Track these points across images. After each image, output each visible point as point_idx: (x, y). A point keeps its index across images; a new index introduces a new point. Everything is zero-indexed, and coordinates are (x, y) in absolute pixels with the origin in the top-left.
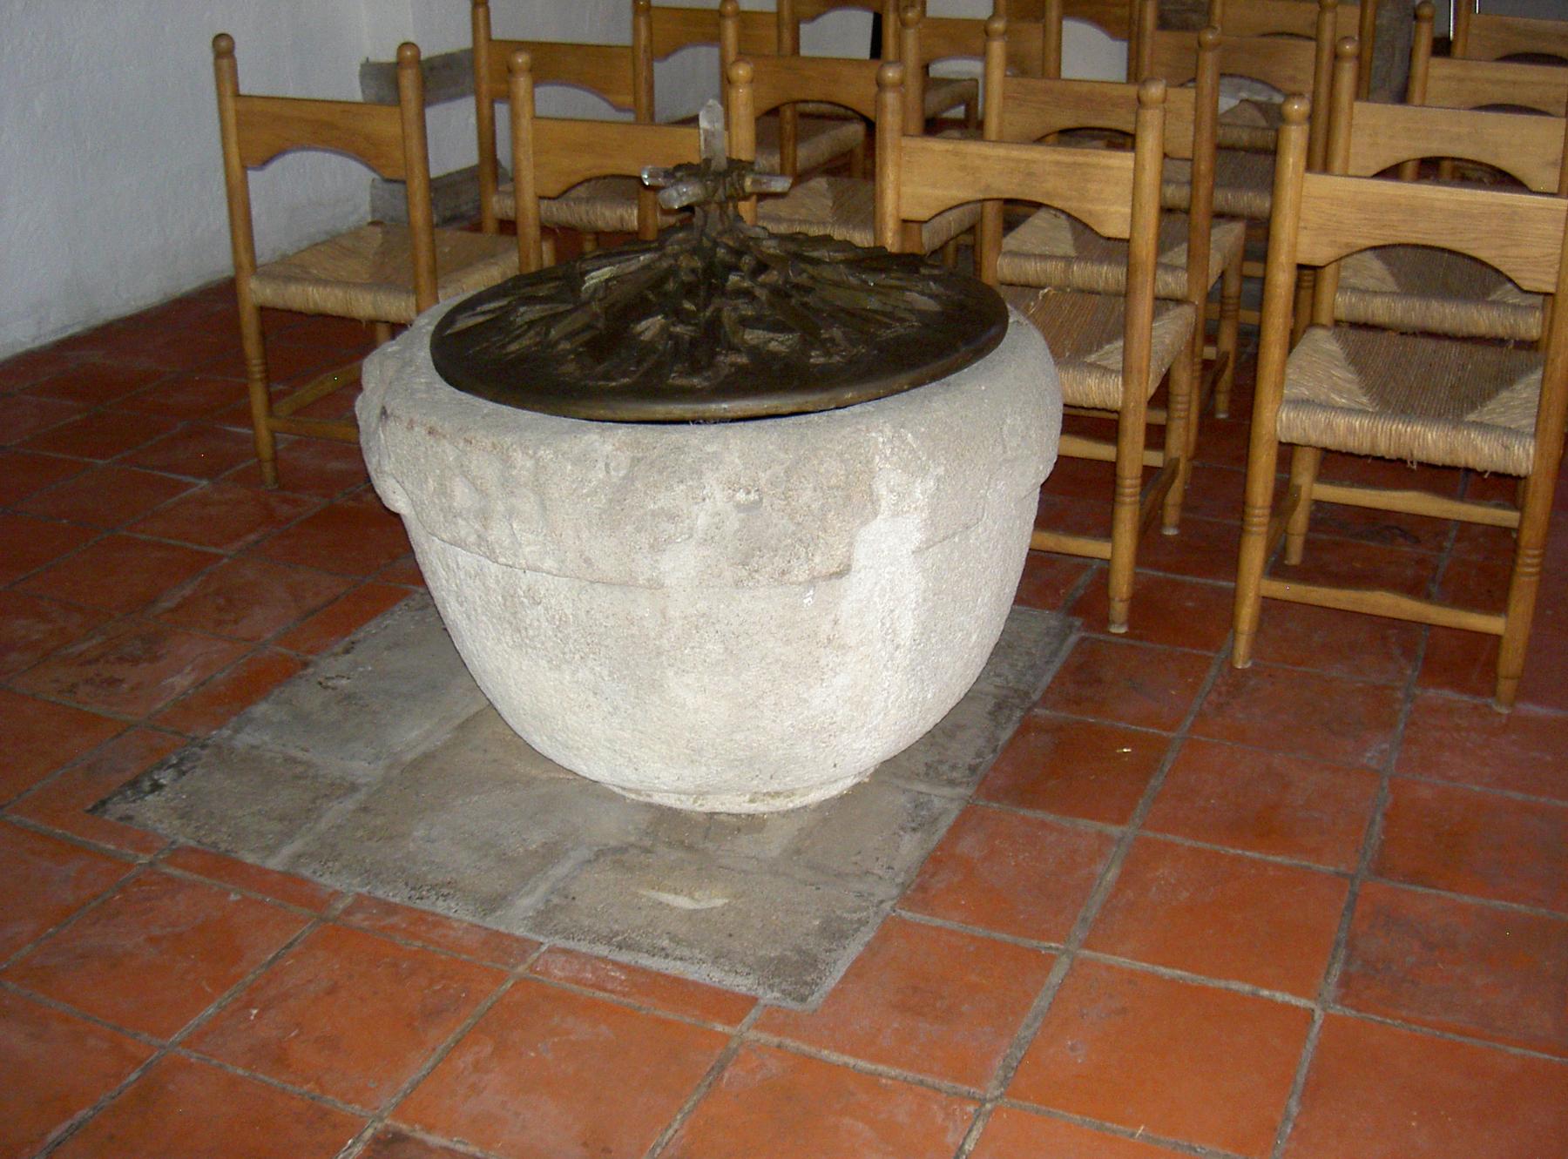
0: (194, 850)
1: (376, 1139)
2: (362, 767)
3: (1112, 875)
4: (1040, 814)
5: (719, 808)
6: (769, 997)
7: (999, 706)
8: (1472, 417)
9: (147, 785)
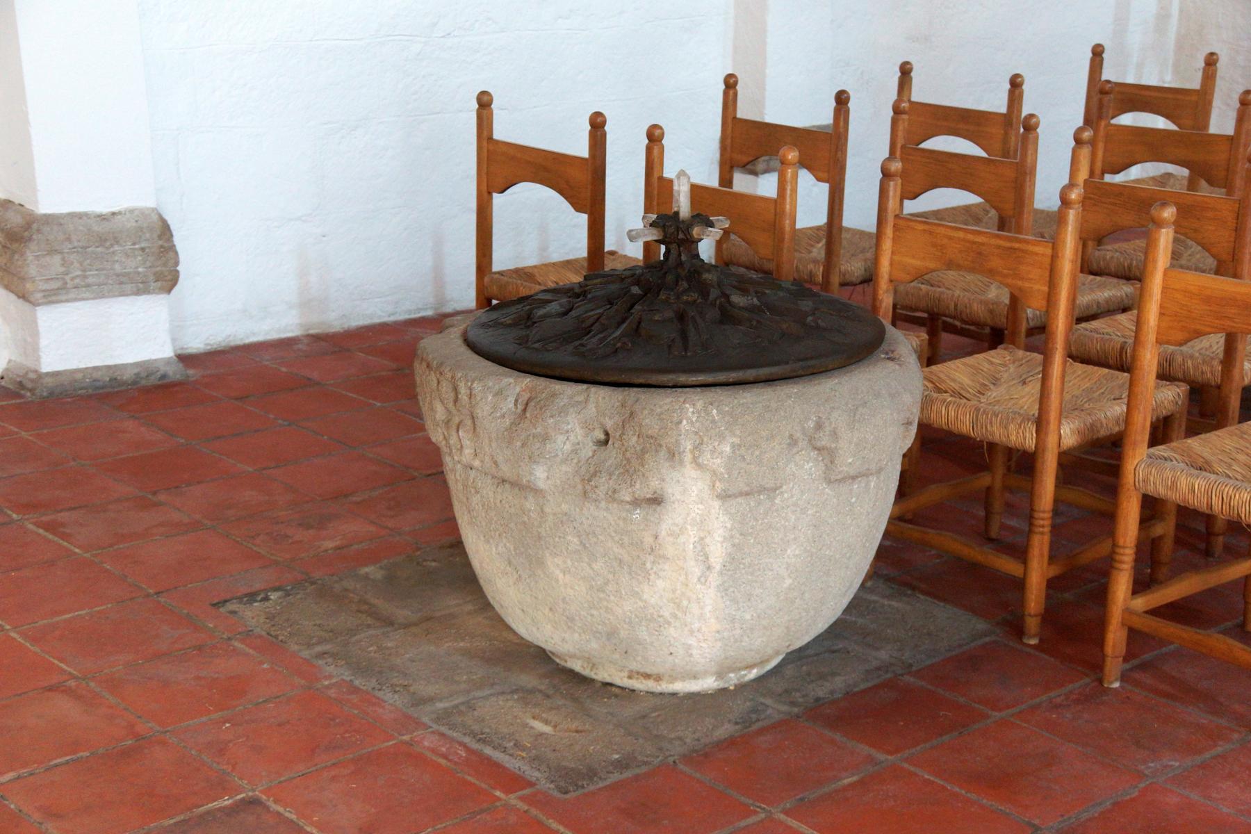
6: (545, 785)
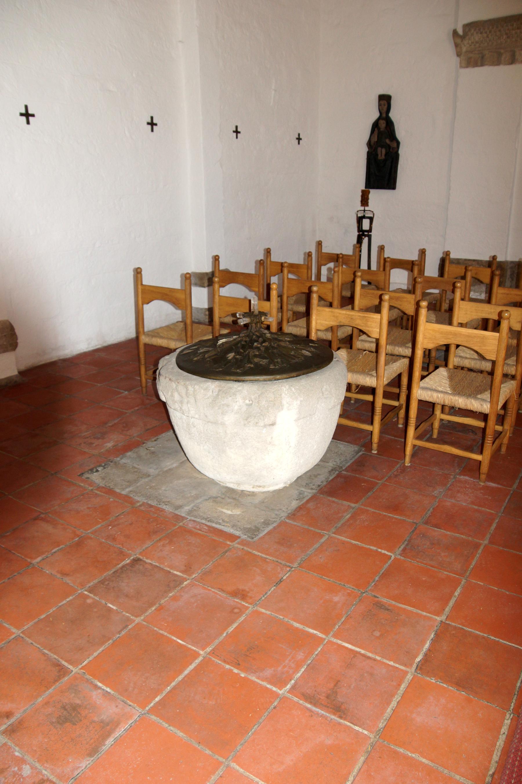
0: (103, 487)
1: (134, 559)
2: (152, 471)
3: (348, 516)
4: (334, 499)
5: (244, 489)
6: (244, 537)
7: (332, 470)
8: (479, 396)
9: (95, 470)
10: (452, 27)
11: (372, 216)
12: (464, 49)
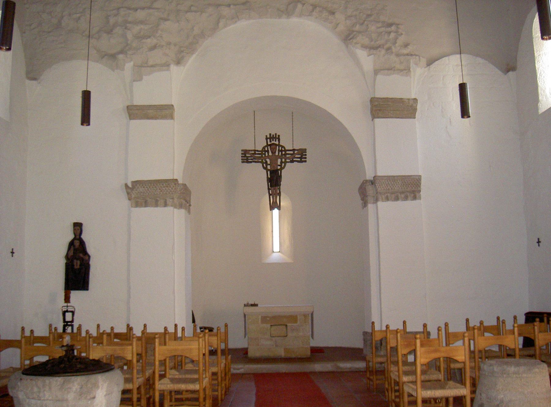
10: (123, 182)
11: (73, 310)
12: (133, 196)
